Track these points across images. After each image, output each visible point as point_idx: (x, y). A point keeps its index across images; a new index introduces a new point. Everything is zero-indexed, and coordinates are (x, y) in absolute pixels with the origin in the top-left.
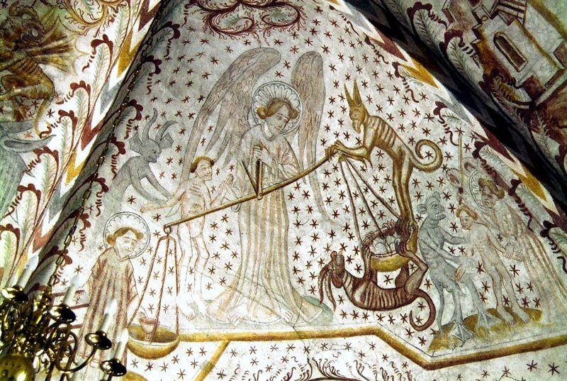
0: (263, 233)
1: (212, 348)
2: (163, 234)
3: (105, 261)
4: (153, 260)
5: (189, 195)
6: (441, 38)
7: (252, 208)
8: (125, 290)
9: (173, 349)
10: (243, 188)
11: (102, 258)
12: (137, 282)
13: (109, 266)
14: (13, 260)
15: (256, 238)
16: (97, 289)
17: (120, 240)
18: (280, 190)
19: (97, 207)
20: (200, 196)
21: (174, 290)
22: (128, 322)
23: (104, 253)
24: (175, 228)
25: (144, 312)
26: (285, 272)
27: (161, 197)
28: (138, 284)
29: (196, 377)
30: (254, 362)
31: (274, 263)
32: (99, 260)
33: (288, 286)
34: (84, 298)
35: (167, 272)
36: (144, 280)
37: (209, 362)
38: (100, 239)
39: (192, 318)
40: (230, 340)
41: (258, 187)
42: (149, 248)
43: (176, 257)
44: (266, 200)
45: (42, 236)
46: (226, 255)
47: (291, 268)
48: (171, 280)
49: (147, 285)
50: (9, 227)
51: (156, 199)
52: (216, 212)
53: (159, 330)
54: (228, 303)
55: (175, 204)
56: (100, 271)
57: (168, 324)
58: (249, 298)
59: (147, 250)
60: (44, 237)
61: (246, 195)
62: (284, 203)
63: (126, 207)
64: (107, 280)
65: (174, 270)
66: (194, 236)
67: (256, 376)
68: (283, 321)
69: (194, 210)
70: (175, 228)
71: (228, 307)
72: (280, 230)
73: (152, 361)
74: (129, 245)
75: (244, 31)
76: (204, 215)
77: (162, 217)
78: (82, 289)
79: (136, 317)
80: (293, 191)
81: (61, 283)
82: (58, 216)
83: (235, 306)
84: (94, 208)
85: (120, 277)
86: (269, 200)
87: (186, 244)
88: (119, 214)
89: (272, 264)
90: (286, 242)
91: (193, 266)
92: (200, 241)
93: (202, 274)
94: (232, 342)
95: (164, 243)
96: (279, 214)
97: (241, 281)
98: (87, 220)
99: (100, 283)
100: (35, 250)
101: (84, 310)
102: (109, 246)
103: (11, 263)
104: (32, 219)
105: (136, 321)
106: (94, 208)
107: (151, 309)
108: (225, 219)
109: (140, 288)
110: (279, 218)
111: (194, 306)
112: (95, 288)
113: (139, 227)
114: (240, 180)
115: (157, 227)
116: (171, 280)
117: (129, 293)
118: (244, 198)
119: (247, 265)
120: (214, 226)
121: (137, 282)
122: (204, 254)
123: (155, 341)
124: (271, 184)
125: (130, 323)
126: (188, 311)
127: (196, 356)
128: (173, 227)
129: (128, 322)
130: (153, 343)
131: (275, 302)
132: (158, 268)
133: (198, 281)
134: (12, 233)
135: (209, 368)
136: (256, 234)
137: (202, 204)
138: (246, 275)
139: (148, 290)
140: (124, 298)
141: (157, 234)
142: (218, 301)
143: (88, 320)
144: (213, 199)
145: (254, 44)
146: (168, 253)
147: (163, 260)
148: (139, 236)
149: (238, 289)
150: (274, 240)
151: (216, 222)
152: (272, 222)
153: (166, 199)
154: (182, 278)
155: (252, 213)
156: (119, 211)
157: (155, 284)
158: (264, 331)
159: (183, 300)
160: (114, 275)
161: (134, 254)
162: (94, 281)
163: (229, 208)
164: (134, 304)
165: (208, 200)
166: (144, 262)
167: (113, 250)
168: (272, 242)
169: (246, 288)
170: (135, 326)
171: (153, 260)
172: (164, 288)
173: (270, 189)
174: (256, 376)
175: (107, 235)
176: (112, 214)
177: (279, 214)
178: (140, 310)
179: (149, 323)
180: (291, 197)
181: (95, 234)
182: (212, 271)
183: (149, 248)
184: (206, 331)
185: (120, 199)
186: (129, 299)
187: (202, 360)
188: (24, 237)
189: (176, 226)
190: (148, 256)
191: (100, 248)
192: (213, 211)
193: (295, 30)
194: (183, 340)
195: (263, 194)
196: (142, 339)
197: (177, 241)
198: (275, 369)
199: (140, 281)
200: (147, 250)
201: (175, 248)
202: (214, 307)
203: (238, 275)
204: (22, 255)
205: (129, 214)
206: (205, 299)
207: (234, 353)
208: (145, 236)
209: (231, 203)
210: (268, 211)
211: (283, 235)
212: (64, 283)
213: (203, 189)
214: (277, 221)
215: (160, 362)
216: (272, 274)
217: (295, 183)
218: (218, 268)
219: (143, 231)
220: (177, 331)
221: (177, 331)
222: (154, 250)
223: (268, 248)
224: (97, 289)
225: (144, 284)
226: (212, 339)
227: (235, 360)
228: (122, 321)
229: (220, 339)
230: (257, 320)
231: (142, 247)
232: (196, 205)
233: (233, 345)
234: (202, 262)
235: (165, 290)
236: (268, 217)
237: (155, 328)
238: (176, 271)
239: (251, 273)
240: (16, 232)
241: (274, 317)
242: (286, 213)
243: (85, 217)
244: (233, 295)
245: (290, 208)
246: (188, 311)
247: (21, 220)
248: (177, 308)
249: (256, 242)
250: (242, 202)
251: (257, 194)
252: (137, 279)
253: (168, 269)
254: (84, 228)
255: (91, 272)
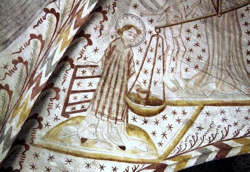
0: (223, 38)
1: (190, 111)
2: (154, 33)
3: (115, 46)
4: (147, 49)
5: (172, 9)
6: (224, 2)
7: (215, 22)
8: (127, 69)
9: (162, 110)
10: (208, 9)
11: (113, 44)
12: (135, 64)
13: (117, 51)
14: (52, 36)
15: (218, 40)
16: (107, 66)
17: (125, 33)
18: (234, 11)
19: (113, 7)
20: (178, 10)
21: (161, 71)
22: (128, 91)
23: (114, 41)
24: (162, 29)
25: (139, 84)
26: (241, 63)
27: (154, 8)
28: (136, 65)
29: (181, 129)
30: (224, 120)
31: (232, 57)
32: (110, 45)
33: (244, 71)
34: (98, 71)
35: (157, 59)
36: (140, 63)
37: (189, 120)
38: (113, 31)
39: (174, 90)
40: (204, 105)
41: (218, 9)
42: (144, 41)
43: (163, 49)
44: (224, 17)
45: (82, 18)
46: (198, 51)
47: (245, 60)
48: (159, 64)
49: (142, 66)
50: (53, 11)
51: (151, 8)
52: (190, 22)
53: (150, 97)
54: (201, 81)
55: (163, 14)
56: (110, 53)
57: (157, 94)
58: (217, 78)
59: (143, 43)
60: (83, 19)
61: (210, 13)
62: (237, 19)
63: (132, 11)
64: (114, 60)
65: (162, 57)
66: (175, 36)
67: (227, 129)
68: (243, 94)
69: (174, 19)
70: (162, 29)
71: (201, 83)
72: (235, 36)
73: (147, 118)
74: (131, 37)
76: (181, 23)
77: (155, 21)
78: (97, 64)
79: (134, 87)
80: (244, 12)
81: (83, 58)
82: (94, 5)
83: (206, 84)
84: (111, 8)
85: (123, 60)
86: (226, 17)
87: (170, 41)
88: (126, 15)
89: (231, 57)
90: (240, 44)
91: (175, 56)
92: (179, 40)
93: (181, 61)
94: (206, 106)
95: (155, 39)
96: (234, 26)
97: (209, 67)
98: (106, 15)
99: (109, 62)
100: (75, 28)
101: (98, 80)
102: (118, 36)
103: (50, 39)
104: (69, 8)
105: (134, 91)
106: (111, 8)
107: (145, 82)
108: (196, 27)
109: (137, 68)
110: (234, 28)
111: (175, 82)
112: (106, 65)
113: (138, 25)
114: (206, 3)
115: (150, 27)
116: (159, 64)
117: (129, 71)
118: (208, 15)
119: (213, 57)
120: (189, 31)
121: (135, 64)
122: (182, 49)
123: (148, 105)
124: (228, 7)
125: (129, 92)
126: (171, 85)
127: (180, 116)
128: (161, 29)
129: (128, 91)
130: (147, 106)
131: (236, 81)
132: (151, 55)
133: (179, 66)
134: (54, 16)
135: (190, 123)
136: (218, 39)
137: (180, 16)
138: (213, 64)
139: (143, 70)
140: (126, 74)
141: (150, 32)
142: (194, 80)
143: (100, 87)
144: (187, 14)
146: (157, 45)
147: (154, 50)
148: (139, 32)
149: (208, 72)
150: (232, 43)
151: (190, 29)
152: (229, 31)
153: (157, 9)
154: (167, 64)
155: (214, 25)
156: (127, 13)
157: (148, 66)
158: (230, 100)
159: (168, 78)
160: (120, 57)
161: (134, 44)
162: (106, 60)
163: (199, 21)
164: (133, 79)
165: (184, 14)
166: (141, 50)
167: (120, 39)
168: (229, 44)
169: (214, 72)
170: (133, 94)
171: (147, 49)
172: (154, 69)
173: (227, 10)
174: (227, 129)
175: (118, 28)
176: (122, 14)
177: (234, 26)
178: (137, 83)
179: (143, 92)
180: (242, 15)
181: (110, 26)
182: (188, 60)
183: (144, 41)
184: (185, 99)
185: (128, 4)
186: (129, 75)
187: (184, 118)
188: (62, 20)
189: (164, 29)
190: (144, 47)
191: (112, 37)
192: (188, 22)
194: (168, 105)
195: (222, 13)
196: (139, 103)
197: (164, 38)
198: (240, 124)
199: (137, 63)
200: (143, 43)
201: (163, 43)
202: (191, 83)
203: (207, 63)
204: (58, 33)
205: (133, 16)
206: (184, 78)
207: (208, 114)
208: (143, 32)
209: (199, 17)
210: (226, 24)
211: (238, 40)
212: (85, 59)
213: (181, 6)
214: (232, 30)
215: (153, 118)
216: (232, 64)
217: (246, 7)
218: (193, 58)
219: (142, 29)
220: (164, 98)
221: (164, 98)
222: (148, 42)
223: (227, 47)
224: (107, 66)
225: (140, 66)
226: (190, 104)
227: (210, 119)
228: (124, 89)
229: (197, 105)
230: (224, 92)
231: (140, 40)
232: (176, 16)
233: (207, 109)
234: (181, 53)
235: (155, 70)
236: (226, 28)
237: (148, 96)
238: (163, 58)
239: (217, 63)
240: (57, 15)
241: (236, 91)
242: (239, 26)
243: (105, 13)
244: (205, 76)
245: (242, 23)
246: (171, 85)
247: (62, 8)
248: (164, 83)
249: (218, 43)
250: (207, 17)
251: (218, 13)
252: (135, 61)
253: (157, 56)
254: (103, 21)
255: (104, 53)
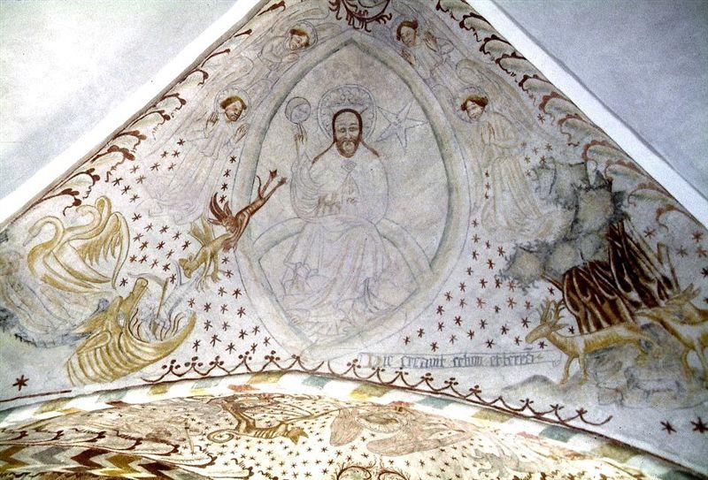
75: (389, 472)
145: (386, 459)
156: (451, 146)
193: (347, 463)
